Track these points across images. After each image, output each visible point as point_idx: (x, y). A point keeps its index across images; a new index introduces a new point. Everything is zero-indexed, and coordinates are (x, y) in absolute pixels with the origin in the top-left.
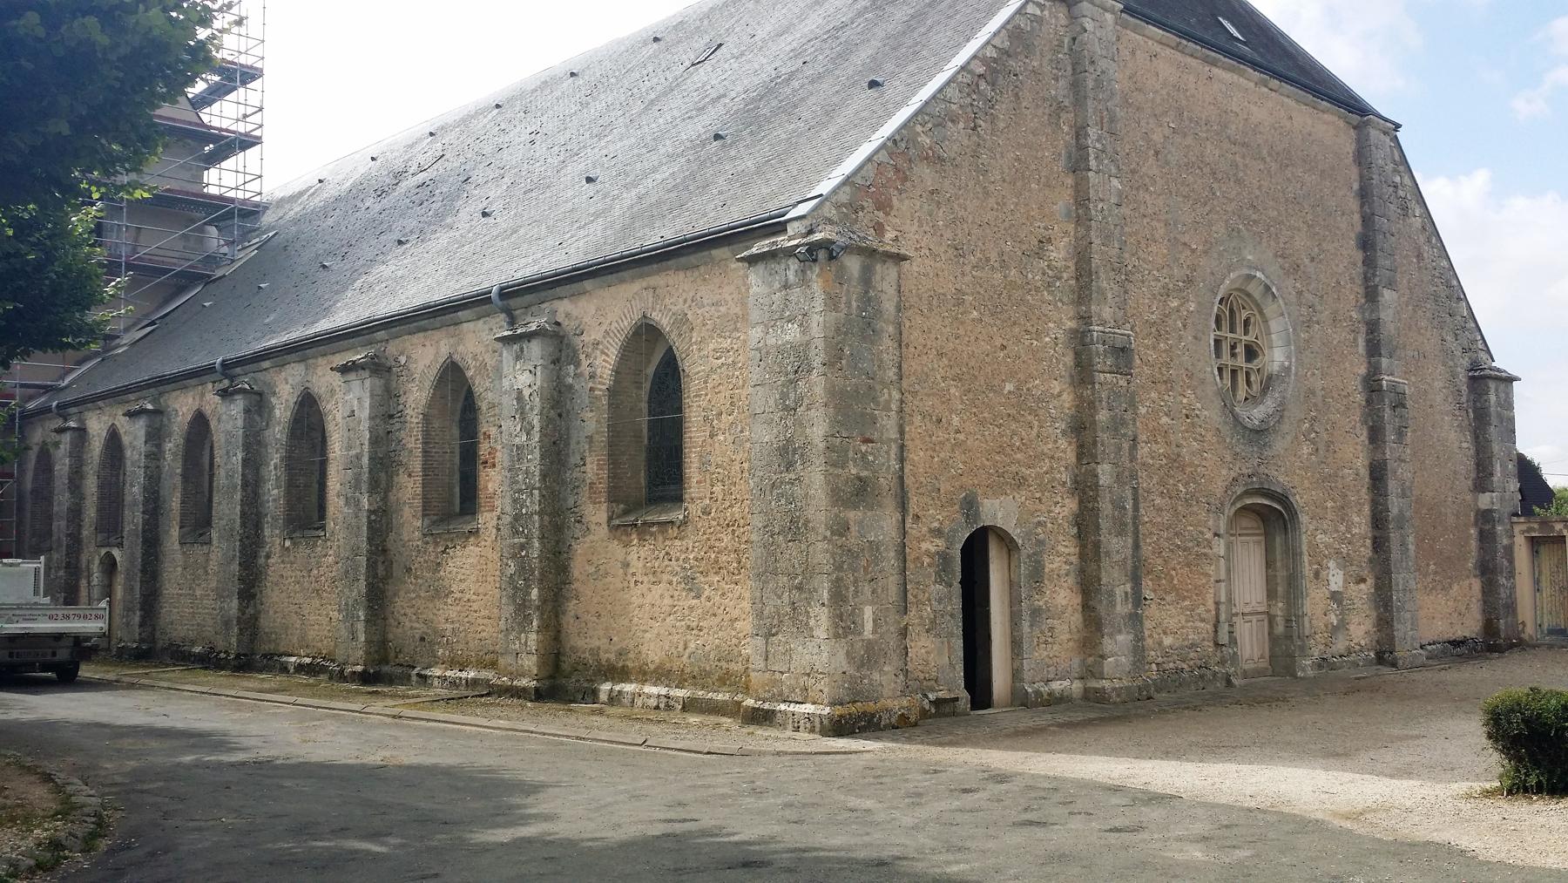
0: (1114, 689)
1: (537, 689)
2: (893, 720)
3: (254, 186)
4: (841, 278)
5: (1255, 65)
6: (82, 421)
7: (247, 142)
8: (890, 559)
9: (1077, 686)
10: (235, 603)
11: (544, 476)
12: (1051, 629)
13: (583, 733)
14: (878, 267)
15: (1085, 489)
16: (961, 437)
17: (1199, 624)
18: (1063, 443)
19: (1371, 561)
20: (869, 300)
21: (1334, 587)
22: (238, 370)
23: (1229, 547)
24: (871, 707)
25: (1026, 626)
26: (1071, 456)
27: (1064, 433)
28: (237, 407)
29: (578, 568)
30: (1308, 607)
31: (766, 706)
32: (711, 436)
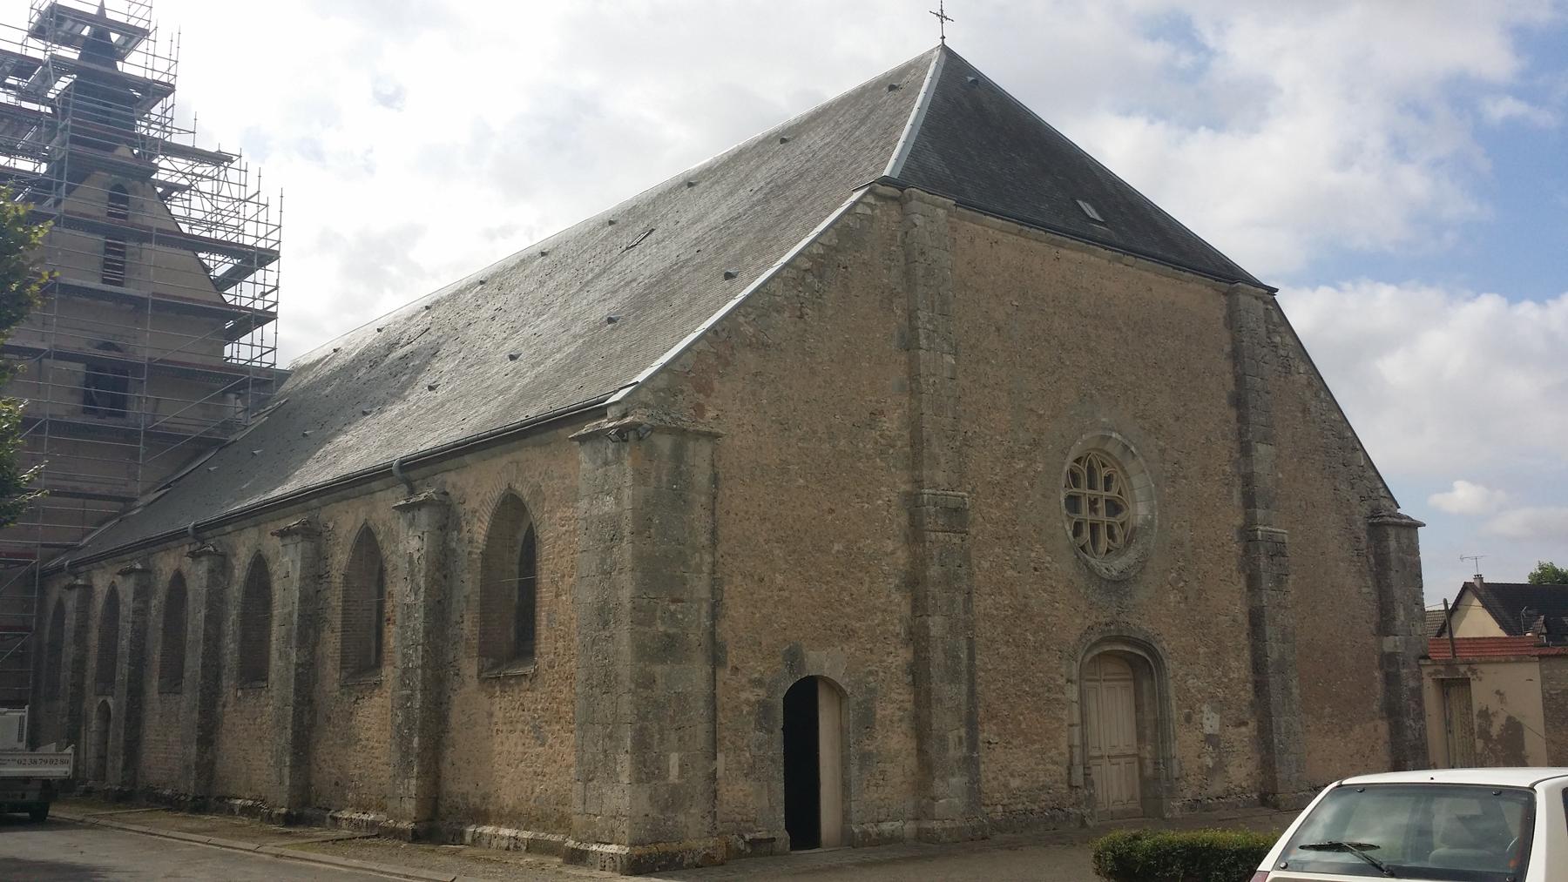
0: (944, 829)
1: (414, 831)
3: (268, 358)
5: (1076, 235)
6: (89, 579)
7: (266, 317)
8: (700, 708)
9: (909, 827)
10: (194, 749)
11: (427, 633)
14: (691, 444)
15: (917, 638)
16: (786, 594)
17: (1050, 766)
19: (1252, 704)
20: (680, 473)
21: (1208, 730)
22: (208, 534)
23: (1082, 694)
24: (675, 847)
25: (854, 770)
26: (906, 609)
27: (898, 588)
29: (455, 718)
30: (1176, 749)
31: (582, 847)
32: (557, 596)
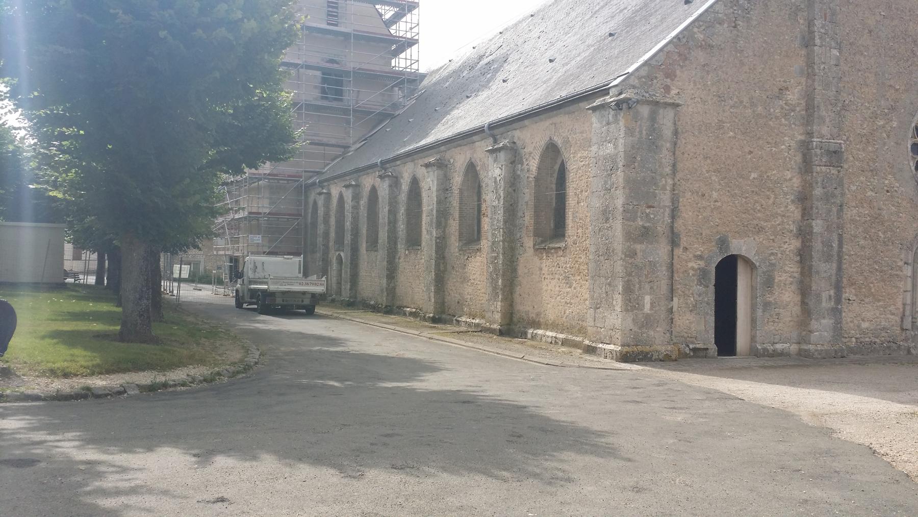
0: (816, 350)
2: (661, 357)
3: (415, 66)
4: (636, 117)
6: (329, 190)
7: (411, 43)
8: (663, 272)
9: (794, 348)
11: (505, 222)
12: (778, 314)
13: (499, 351)
14: (661, 111)
15: (804, 234)
16: (719, 204)
18: (792, 207)
20: (654, 129)
24: (647, 349)
28: (387, 183)
29: (521, 270)
31: (594, 345)
32: (578, 203)
